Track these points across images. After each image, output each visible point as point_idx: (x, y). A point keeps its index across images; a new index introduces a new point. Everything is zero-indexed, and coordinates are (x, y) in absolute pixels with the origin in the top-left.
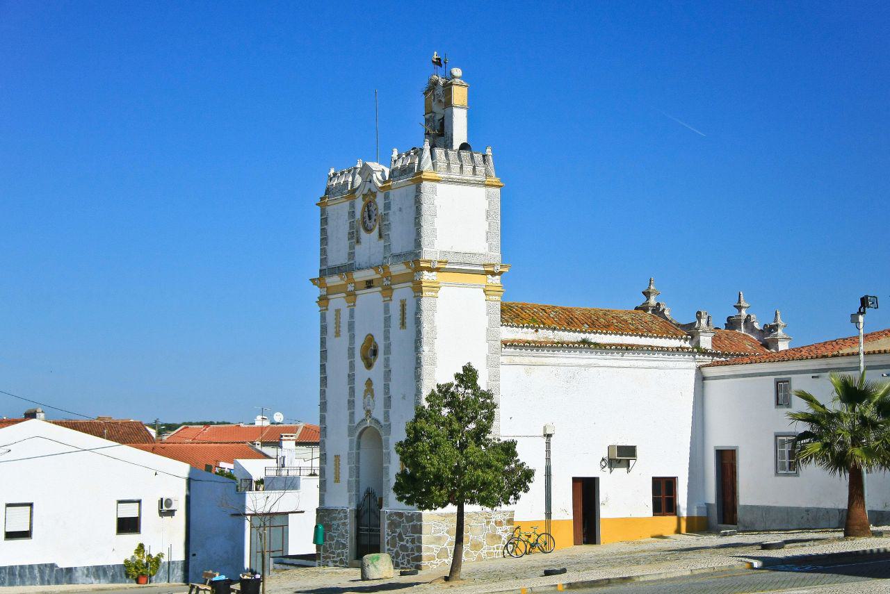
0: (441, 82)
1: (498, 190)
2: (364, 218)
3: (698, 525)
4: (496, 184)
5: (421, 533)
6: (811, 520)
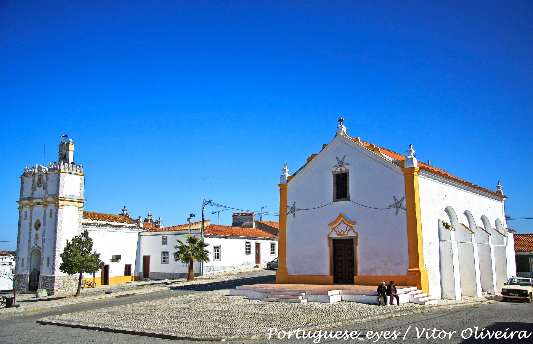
0: (66, 143)
2: (38, 183)
3: (137, 279)
6: (182, 276)
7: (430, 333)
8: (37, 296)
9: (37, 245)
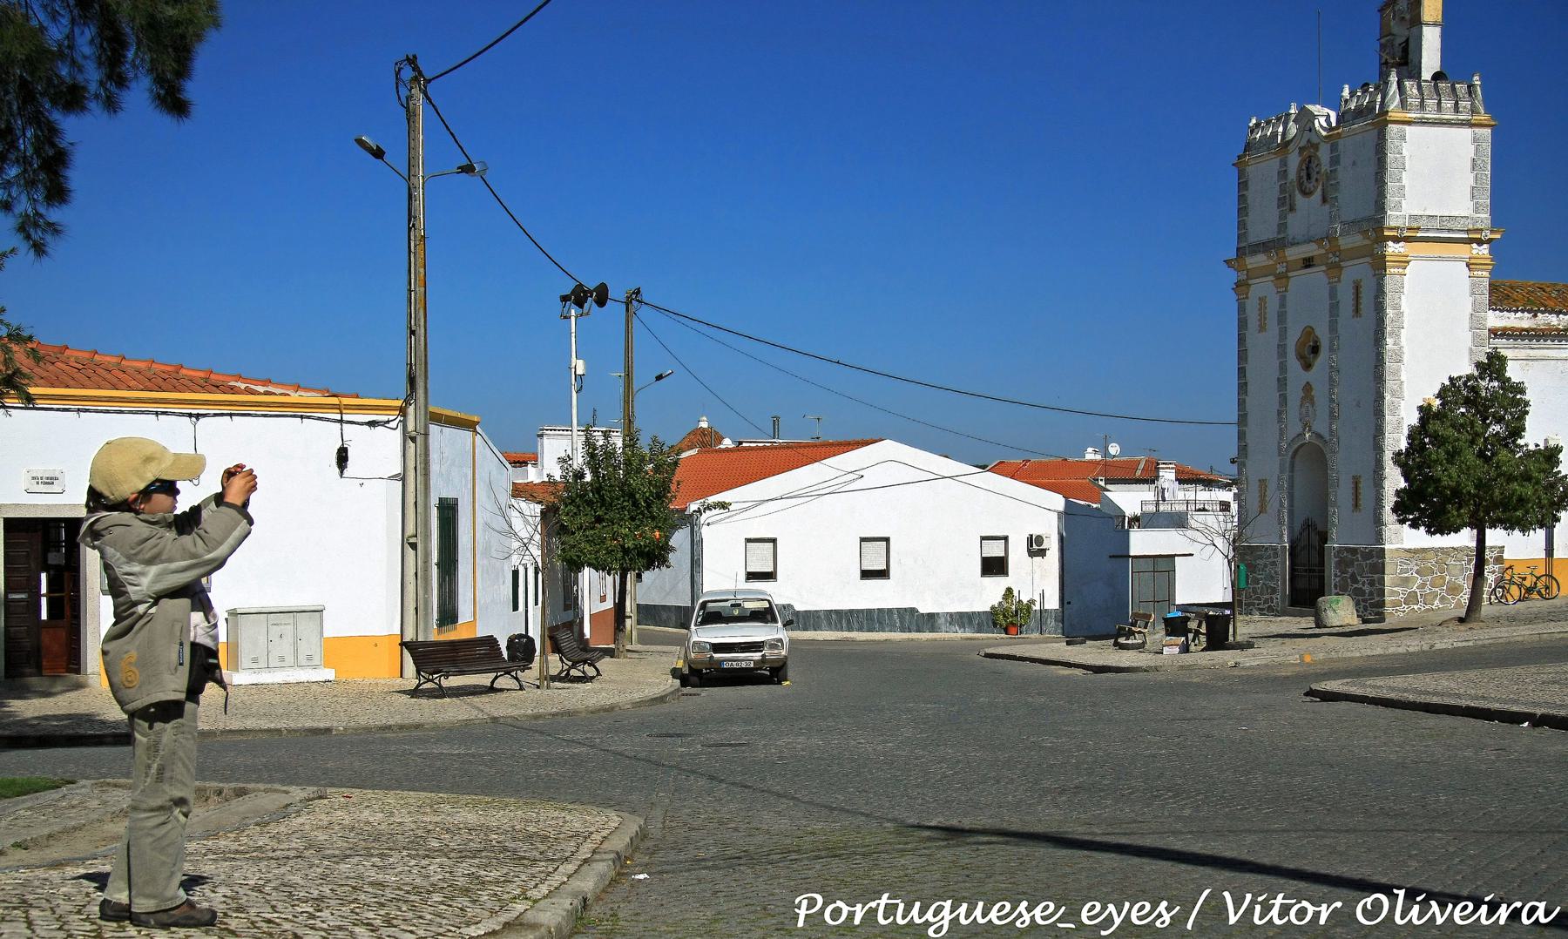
1: (1488, 131)
4: (1486, 122)
5: (1384, 573)
7: (1267, 908)
8: (1319, 624)
9: (1310, 427)
